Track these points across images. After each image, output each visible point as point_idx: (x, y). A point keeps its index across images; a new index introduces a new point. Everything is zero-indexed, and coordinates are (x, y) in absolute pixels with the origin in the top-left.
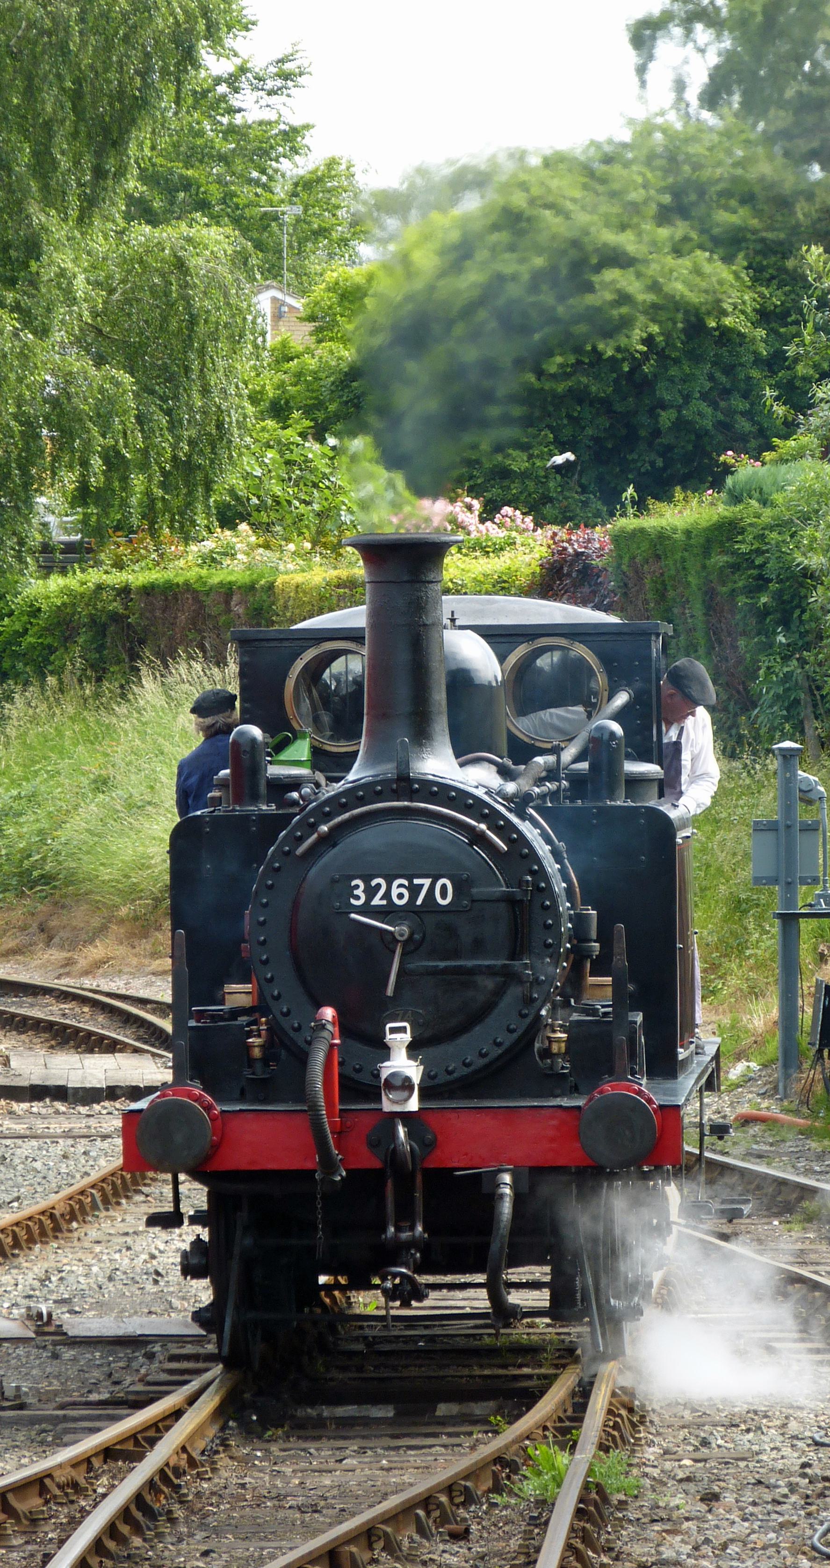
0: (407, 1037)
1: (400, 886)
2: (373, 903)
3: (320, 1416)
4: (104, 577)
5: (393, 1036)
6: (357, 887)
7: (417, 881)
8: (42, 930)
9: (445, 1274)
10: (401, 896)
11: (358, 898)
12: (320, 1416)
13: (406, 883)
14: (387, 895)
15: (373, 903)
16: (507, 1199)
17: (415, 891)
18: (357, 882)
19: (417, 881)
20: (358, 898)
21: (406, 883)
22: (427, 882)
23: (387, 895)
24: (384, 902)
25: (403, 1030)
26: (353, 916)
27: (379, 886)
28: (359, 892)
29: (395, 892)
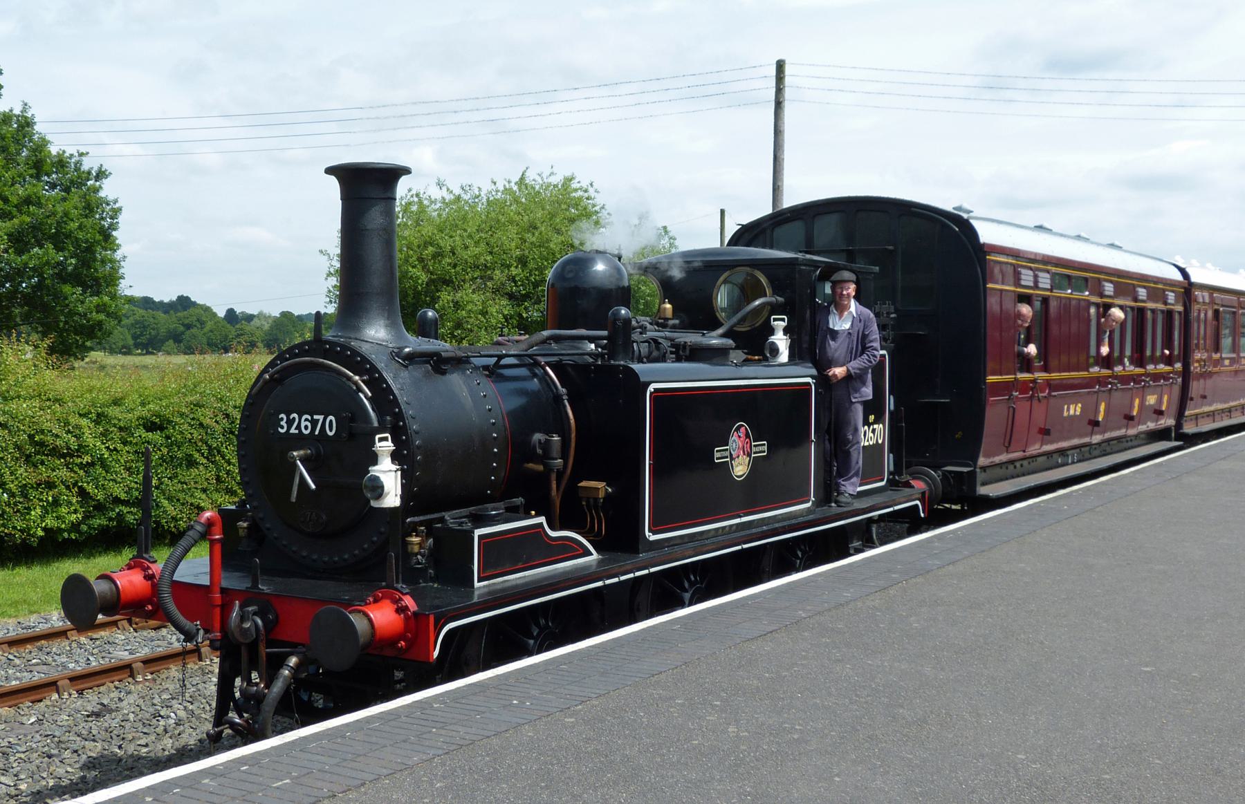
0: (783, 324)
1: (306, 420)
2: (291, 432)
3: (400, 684)
4: (500, 338)
5: (776, 323)
6: (282, 419)
7: (316, 417)
8: (640, 218)
9: (433, 513)
10: (306, 427)
11: (282, 427)
12: (400, 684)
13: (309, 418)
14: (298, 427)
15: (291, 432)
16: (565, 397)
17: (314, 423)
18: (282, 415)
19: (316, 417)
20: (282, 427)
21: (309, 418)
22: (321, 418)
23: (298, 427)
24: (297, 431)
25: (783, 320)
26: (317, 433)
27: (294, 418)
28: (283, 423)
29: (303, 424)
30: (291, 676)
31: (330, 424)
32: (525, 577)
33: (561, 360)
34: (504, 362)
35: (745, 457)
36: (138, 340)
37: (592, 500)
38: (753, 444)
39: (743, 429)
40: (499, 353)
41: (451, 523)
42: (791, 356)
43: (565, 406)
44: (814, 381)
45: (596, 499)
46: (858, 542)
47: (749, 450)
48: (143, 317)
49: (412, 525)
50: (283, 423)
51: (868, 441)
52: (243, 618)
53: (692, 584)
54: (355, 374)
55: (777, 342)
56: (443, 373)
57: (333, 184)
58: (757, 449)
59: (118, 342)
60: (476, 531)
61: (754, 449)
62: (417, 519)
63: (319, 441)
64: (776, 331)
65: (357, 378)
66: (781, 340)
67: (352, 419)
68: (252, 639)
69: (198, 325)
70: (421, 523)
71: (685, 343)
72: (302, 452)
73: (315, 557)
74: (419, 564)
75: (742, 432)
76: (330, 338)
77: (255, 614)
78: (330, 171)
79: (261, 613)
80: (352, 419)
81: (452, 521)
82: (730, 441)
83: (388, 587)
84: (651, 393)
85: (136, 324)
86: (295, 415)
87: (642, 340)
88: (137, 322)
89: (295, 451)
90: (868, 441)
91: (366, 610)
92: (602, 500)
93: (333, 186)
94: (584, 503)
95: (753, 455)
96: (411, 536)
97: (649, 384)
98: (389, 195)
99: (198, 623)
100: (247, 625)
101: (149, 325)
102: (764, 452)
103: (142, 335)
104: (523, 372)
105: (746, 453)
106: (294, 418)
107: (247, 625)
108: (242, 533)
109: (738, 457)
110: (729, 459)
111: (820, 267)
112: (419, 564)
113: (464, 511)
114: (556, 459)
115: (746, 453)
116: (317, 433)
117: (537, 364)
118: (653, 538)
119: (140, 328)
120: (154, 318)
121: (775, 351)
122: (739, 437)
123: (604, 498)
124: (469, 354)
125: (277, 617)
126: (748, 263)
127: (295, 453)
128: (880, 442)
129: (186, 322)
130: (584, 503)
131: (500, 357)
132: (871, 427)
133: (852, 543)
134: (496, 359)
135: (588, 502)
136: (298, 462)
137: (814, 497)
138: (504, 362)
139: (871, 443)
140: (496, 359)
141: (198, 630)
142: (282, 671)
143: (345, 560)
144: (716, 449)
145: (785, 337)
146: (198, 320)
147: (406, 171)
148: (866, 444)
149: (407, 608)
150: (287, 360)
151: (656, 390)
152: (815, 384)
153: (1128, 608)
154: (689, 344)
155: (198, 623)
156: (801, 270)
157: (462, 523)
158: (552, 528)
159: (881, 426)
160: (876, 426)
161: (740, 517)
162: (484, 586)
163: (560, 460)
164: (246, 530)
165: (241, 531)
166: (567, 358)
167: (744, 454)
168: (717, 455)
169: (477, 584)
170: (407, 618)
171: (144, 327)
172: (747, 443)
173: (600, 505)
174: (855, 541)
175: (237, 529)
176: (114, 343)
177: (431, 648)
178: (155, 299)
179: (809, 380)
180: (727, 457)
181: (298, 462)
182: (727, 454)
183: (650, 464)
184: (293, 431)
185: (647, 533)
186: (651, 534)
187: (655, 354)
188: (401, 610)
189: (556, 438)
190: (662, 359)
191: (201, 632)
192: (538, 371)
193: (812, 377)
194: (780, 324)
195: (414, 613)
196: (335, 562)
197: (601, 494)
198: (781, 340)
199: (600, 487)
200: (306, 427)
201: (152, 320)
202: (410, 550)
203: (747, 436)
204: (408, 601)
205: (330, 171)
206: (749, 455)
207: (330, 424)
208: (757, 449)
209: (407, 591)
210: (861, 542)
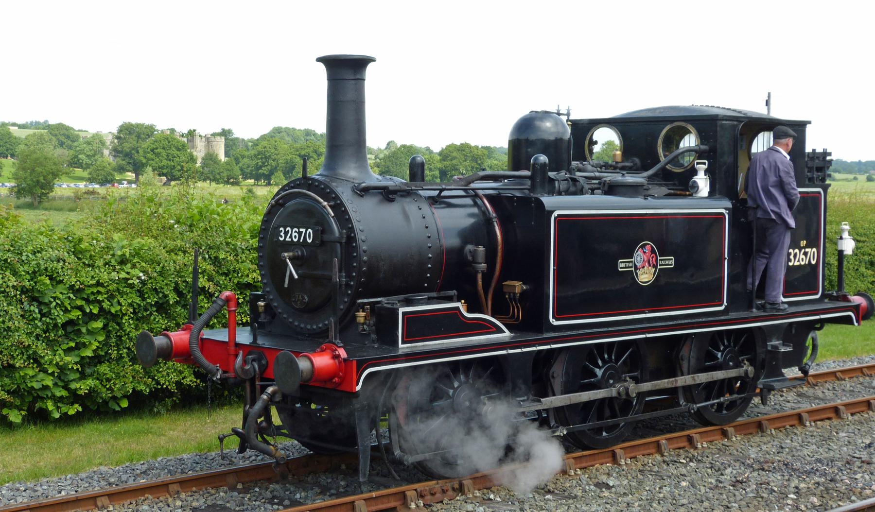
0: (705, 167)
1: (295, 232)
2: (287, 240)
5: (698, 166)
6: (282, 231)
7: (301, 230)
10: (295, 237)
11: (282, 237)
14: (291, 237)
15: (287, 240)
17: (300, 233)
18: (282, 229)
19: (301, 230)
20: (282, 237)
21: (297, 230)
23: (291, 237)
24: (290, 240)
25: (704, 164)
26: (301, 241)
27: (288, 231)
28: (282, 234)
30: (268, 399)
31: (309, 234)
32: (443, 343)
33: (500, 194)
34: (444, 193)
35: (650, 268)
36: (260, 171)
37: (512, 294)
38: (659, 258)
39: (648, 247)
40: (440, 187)
41: (386, 303)
42: (712, 193)
43: (494, 226)
44: (728, 212)
45: (515, 294)
46: (778, 340)
47: (655, 263)
48: (265, 147)
49: (361, 305)
50: (282, 234)
51: (799, 261)
52: (245, 362)
53: (604, 362)
54: (325, 201)
55: (697, 180)
56: (392, 201)
57: (322, 69)
58: (663, 263)
59: (222, 172)
60: (400, 309)
61: (660, 263)
62: (366, 301)
63: (303, 246)
64: (698, 172)
65: (325, 203)
66: (702, 182)
67: (323, 232)
68: (251, 377)
69: (315, 156)
70: (369, 303)
71: (605, 181)
72: (291, 254)
73: (302, 326)
74: (365, 330)
75: (647, 249)
76: (317, 177)
77: (254, 360)
78: (319, 60)
79: (258, 360)
80: (323, 232)
81: (386, 302)
82: (635, 255)
83: (329, 342)
84: (555, 218)
85: (259, 155)
86: (288, 229)
87: (563, 179)
88: (259, 153)
89: (286, 252)
90: (799, 261)
91: (310, 355)
92: (518, 295)
93: (322, 71)
94: (507, 296)
95: (659, 267)
96: (359, 311)
97: (552, 212)
98: (358, 77)
99: (218, 365)
100: (247, 367)
101: (270, 156)
102: (671, 265)
103: (263, 165)
104: (468, 201)
105: (652, 265)
106: (288, 231)
107: (247, 367)
108: (261, 310)
109: (643, 267)
110: (633, 269)
111: (743, 121)
112: (365, 330)
113: (402, 297)
114: (481, 263)
115: (652, 265)
116: (301, 241)
117: (477, 195)
118: (556, 323)
119: (262, 158)
120: (276, 149)
121: (695, 187)
122: (645, 253)
123: (520, 294)
124: (413, 188)
125: (267, 362)
126: (682, 119)
127: (286, 254)
128: (813, 262)
129: (303, 153)
130: (507, 296)
131: (441, 190)
132: (803, 250)
133: (771, 341)
134: (438, 191)
135: (510, 296)
136: (288, 260)
137: (727, 302)
138: (444, 193)
139: (803, 263)
140: (438, 191)
141: (218, 370)
142: (262, 396)
143: (320, 328)
144: (620, 261)
145: (705, 177)
146: (315, 151)
147: (370, 60)
148: (797, 263)
149: (339, 356)
150: (287, 190)
151: (559, 215)
152: (728, 214)
153: (111, 252)
154: (608, 182)
155: (218, 365)
156: (722, 125)
157: (393, 303)
158: (469, 311)
159: (814, 250)
160: (807, 250)
161: (646, 313)
162: (407, 348)
163: (483, 265)
164: (263, 308)
165: (260, 308)
166: (507, 191)
167: (649, 265)
168: (620, 265)
169: (401, 345)
170: (340, 363)
171: (266, 158)
172: (653, 257)
173: (517, 297)
174: (773, 341)
175: (257, 306)
176: (219, 174)
177: (354, 383)
178: (317, 132)
179: (723, 211)
180: (631, 267)
181: (288, 260)
182: (632, 264)
183: (554, 270)
184: (288, 239)
185: (551, 319)
186: (554, 320)
187: (572, 189)
188: (336, 357)
189: (481, 248)
190: (581, 192)
191: (220, 372)
192: (479, 202)
193: (726, 209)
194: (702, 168)
195: (344, 360)
196: (314, 329)
197: (518, 290)
198: (702, 182)
199: (518, 286)
200: (295, 237)
201: (273, 151)
202: (358, 321)
203: (653, 251)
204: (343, 353)
205: (319, 60)
206: (655, 266)
207: (309, 234)
208: (663, 263)
209: (342, 345)
210: (781, 342)
